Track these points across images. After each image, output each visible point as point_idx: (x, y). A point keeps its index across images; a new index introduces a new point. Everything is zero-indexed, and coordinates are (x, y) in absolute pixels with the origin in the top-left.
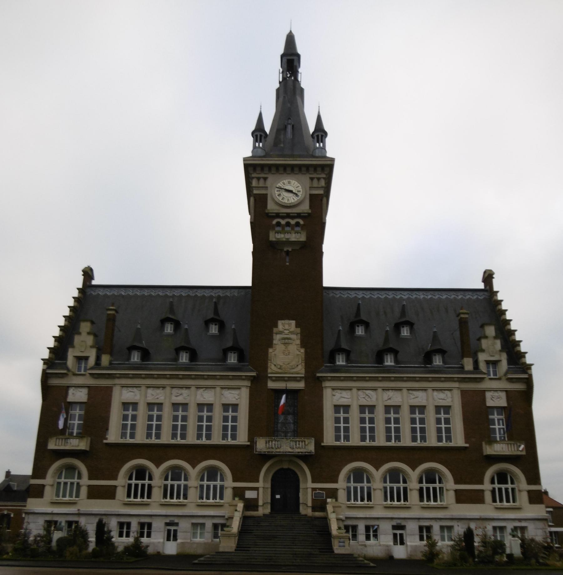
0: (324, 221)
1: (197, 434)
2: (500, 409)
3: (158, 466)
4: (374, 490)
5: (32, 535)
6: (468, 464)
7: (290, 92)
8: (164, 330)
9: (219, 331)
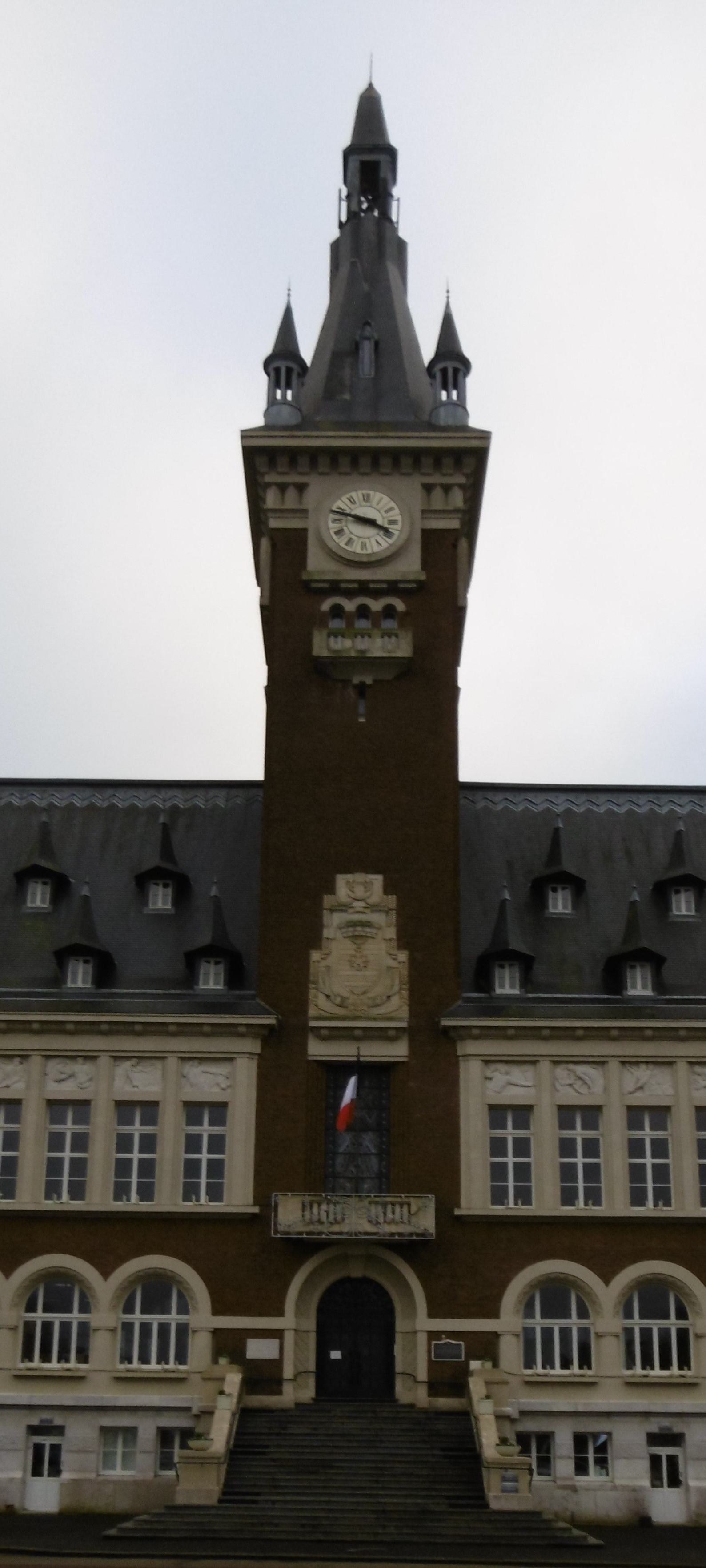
0: (460, 604)
1: (185, 1184)
4: (599, 1336)
7: (368, 252)
8: (25, 902)
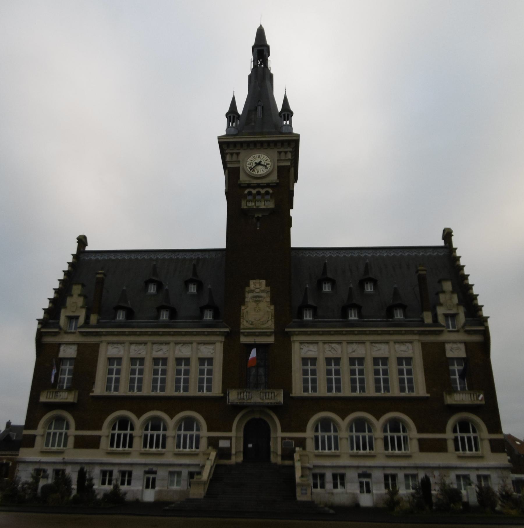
0: (291, 189)
1: (176, 386)
2: (459, 360)
3: (139, 417)
4: (376, 439)
5: (21, 483)
6: (430, 413)
7: (261, 78)
8: (148, 290)
9: (197, 290)
